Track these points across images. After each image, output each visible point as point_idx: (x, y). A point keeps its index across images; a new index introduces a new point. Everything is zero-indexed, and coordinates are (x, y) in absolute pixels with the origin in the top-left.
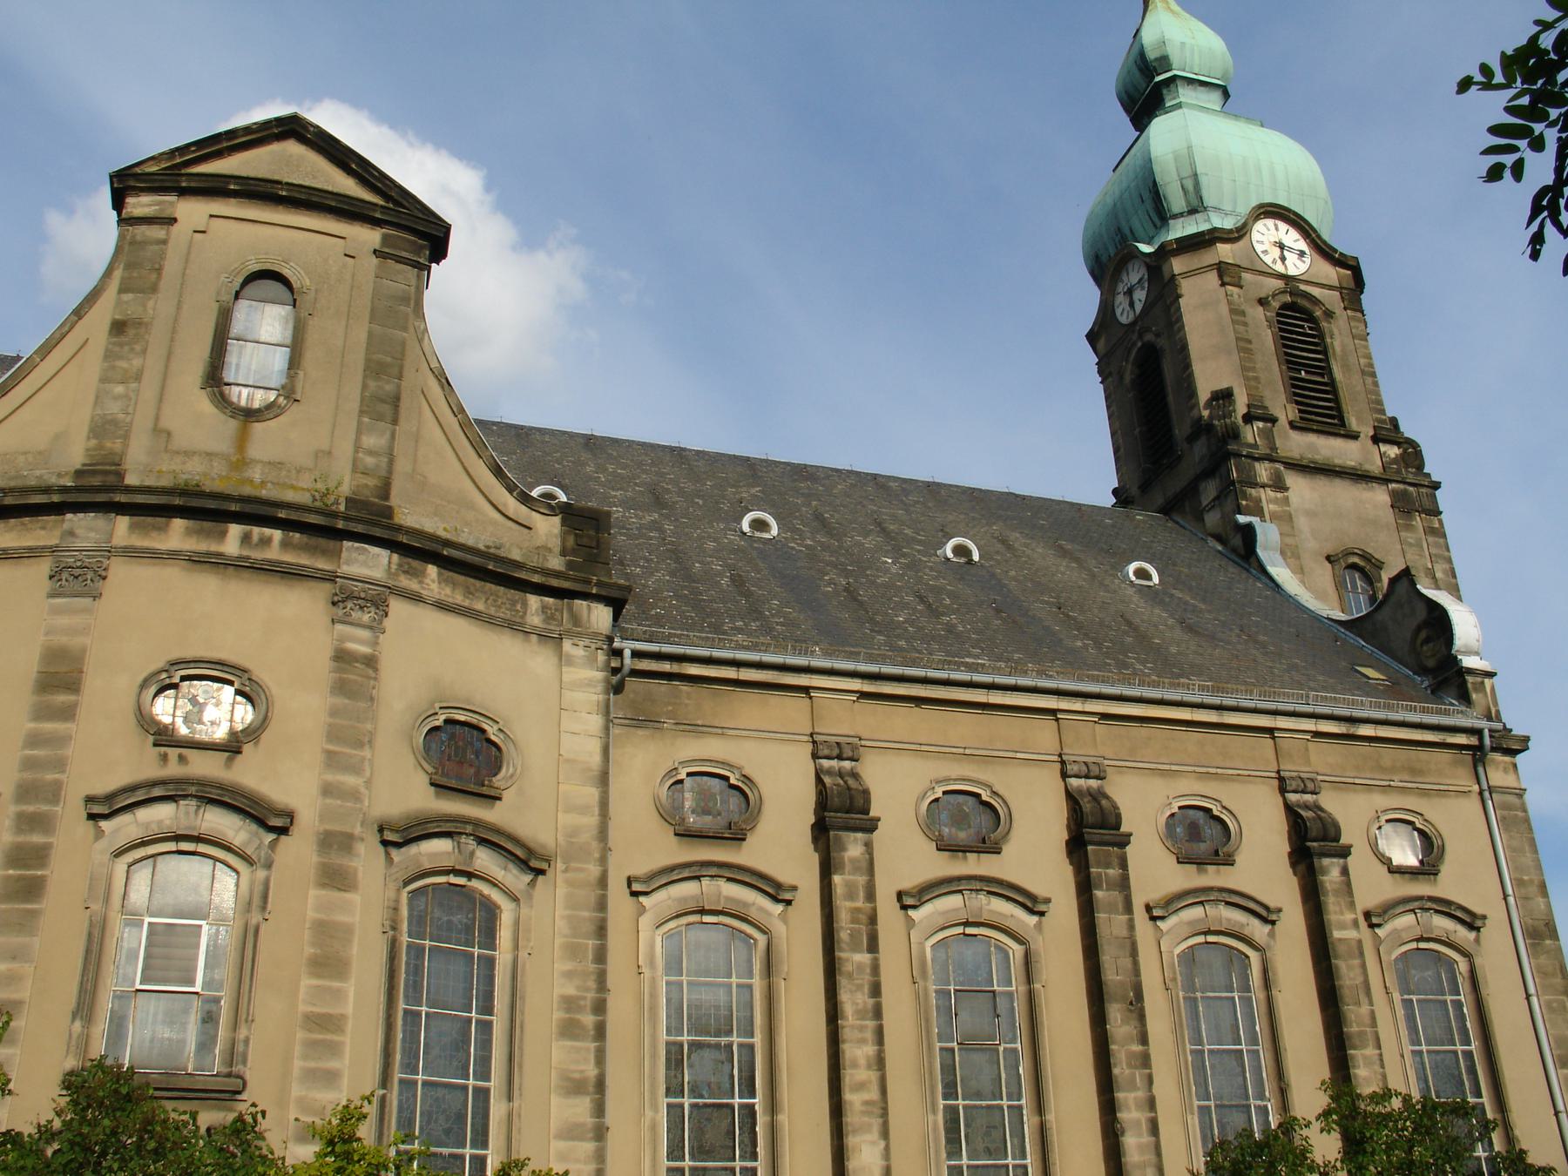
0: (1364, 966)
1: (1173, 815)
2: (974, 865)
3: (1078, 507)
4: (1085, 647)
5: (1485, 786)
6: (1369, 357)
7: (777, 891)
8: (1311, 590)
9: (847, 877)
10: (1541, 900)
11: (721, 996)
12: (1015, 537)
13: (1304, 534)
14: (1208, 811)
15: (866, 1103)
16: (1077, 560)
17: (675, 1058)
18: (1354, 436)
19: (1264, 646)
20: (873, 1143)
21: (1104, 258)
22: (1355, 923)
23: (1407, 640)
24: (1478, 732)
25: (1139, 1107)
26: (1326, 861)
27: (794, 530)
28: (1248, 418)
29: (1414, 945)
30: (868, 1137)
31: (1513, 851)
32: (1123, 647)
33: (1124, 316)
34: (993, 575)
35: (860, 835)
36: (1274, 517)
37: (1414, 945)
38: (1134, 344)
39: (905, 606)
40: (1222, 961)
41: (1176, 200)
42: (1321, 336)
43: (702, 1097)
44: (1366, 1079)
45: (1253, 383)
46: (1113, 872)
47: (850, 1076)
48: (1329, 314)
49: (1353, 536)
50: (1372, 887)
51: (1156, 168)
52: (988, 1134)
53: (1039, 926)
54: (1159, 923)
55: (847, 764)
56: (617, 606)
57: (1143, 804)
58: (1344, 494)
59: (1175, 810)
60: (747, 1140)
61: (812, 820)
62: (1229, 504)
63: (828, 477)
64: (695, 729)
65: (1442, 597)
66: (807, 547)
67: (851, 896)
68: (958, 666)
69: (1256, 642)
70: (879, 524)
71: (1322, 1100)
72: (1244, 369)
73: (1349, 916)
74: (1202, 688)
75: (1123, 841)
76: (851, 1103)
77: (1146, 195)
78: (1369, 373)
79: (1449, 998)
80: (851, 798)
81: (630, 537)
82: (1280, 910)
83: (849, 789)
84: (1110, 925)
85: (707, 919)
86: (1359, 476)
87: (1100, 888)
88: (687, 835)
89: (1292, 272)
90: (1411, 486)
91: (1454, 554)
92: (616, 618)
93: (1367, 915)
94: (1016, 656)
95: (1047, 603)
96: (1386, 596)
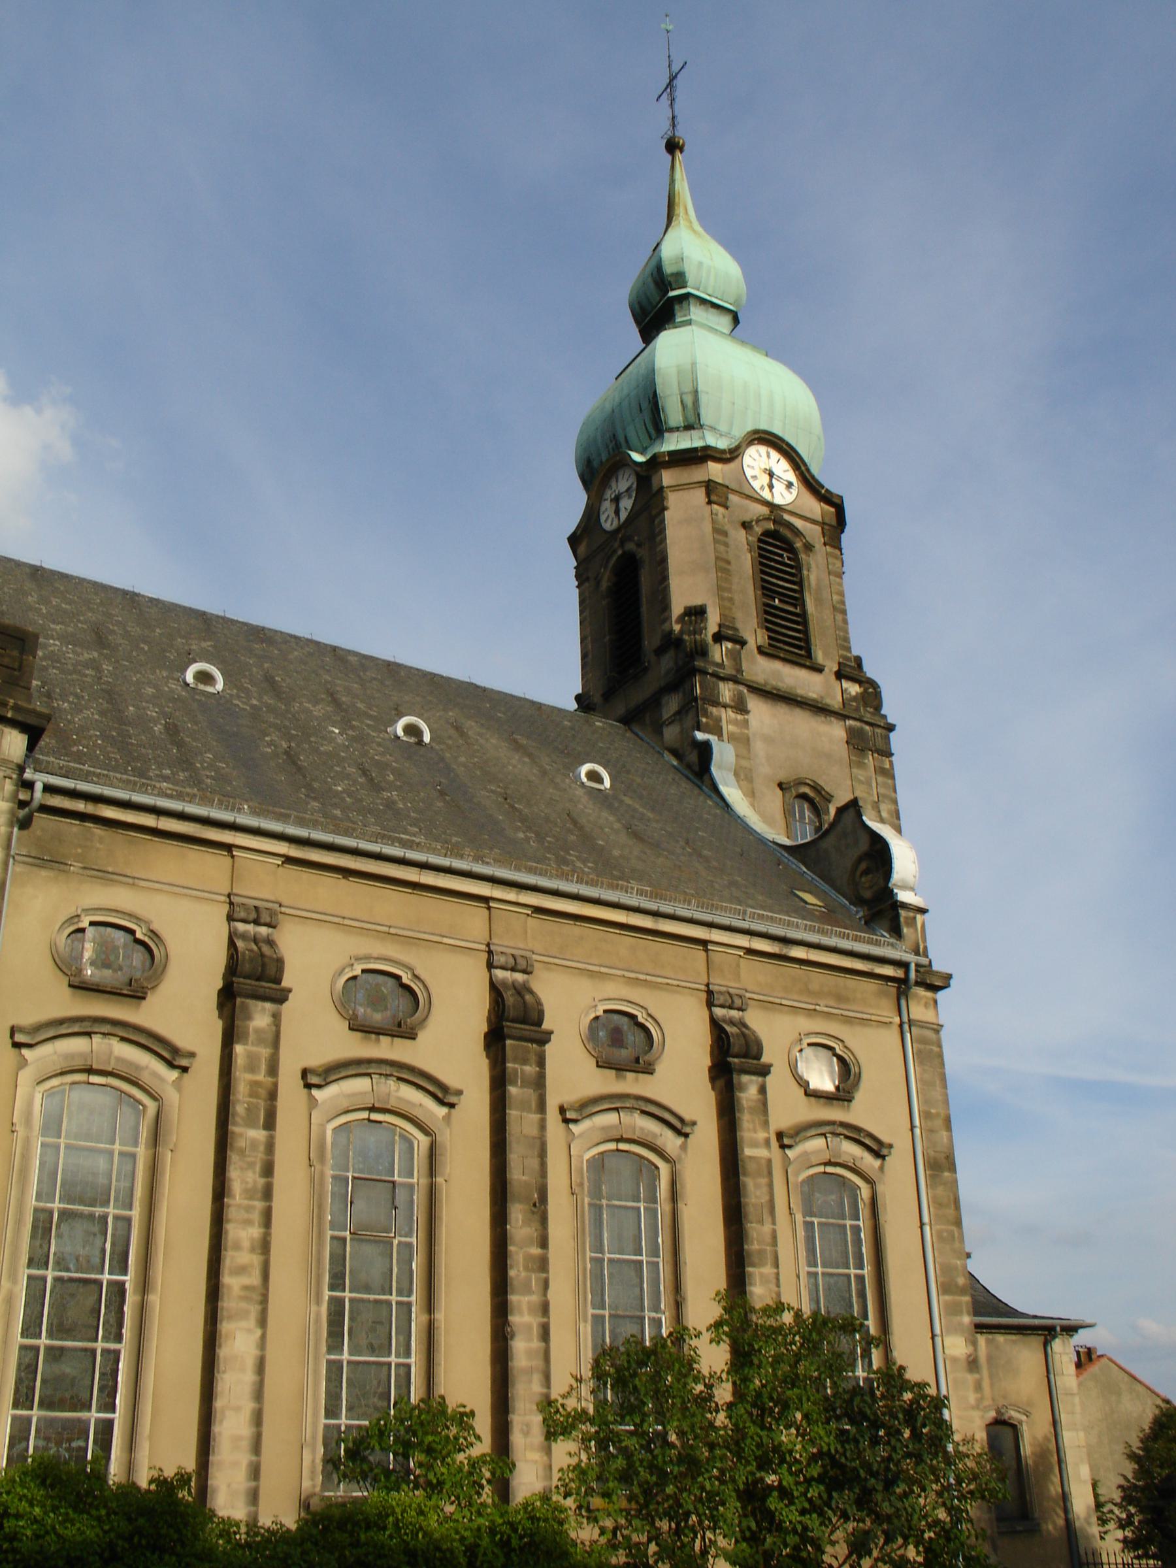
0: (771, 1186)
1: (597, 1018)
2: (386, 1049)
3: (538, 706)
4: (527, 839)
5: (905, 1019)
6: (842, 594)
7: (174, 1057)
8: (760, 814)
9: (250, 1048)
10: (945, 1133)
11: (101, 1163)
12: (472, 727)
13: (760, 757)
14: (633, 1017)
15: (246, 1288)
16: (530, 755)
17: (42, 1227)
18: (819, 669)
19: (707, 860)
20: (249, 1331)
21: (595, 464)
22: (767, 1142)
23: (848, 869)
24: (904, 965)
25: (531, 1311)
26: (745, 1078)
27: (240, 688)
28: (718, 638)
29: (821, 1169)
30: (244, 1324)
31: (924, 1084)
32: (568, 843)
33: (608, 522)
34: (442, 759)
35: (268, 1005)
36: (732, 738)
37: (821, 1169)
38: (615, 551)
39: (348, 776)
40: (631, 1170)
41: (674, 415)
42: (799, 567)
43: (68, 1270)
44: (759, 1293)
45: (727, 604)
46: (530, 1069)
47: (231, 1259)
48: (809, 547)
49: (808, 767)
50: (786, 1108)
51: (658, 380)
52: (373, 1330)
53: (447, 1118)
54: (571, 1126)
55: (263, 930)
56: (34, 734)
57: (568, 1005)
58: (802, 724)
59: (600, 1013)
60: (112, 1321)
61: (220, 984)
62: (689, 721)
63: (286, 642)
64: (104, 876)
65: (885, 831)
66: (252, 706)
67: (252, 1068)
68: (393, 841)
69: (700, 855)
70: (332, 695)
71: (715, 1311)
72: (719, 588)
73: (761, 1135)
74: (640, 893)
75: (544, 1039)
76: (229, 1287)
77: (645, 405)
78: (840, 609)
79: (848, 1223)
80: (264, 965)
81: (62, 671)
82: (694, 1123)
83: (262, 955)
84: (521, 1122)
85: (95, 1079)
86: (818, 709)
87: (514, 1083)
88: (81, 987)
89: (778, 500)
90: (867, 726)
91: (901, 796)
92: (31, 747)
93: (780, 1135)
94: (454, 839)
95: (492, 791)
96: (833, 825)
